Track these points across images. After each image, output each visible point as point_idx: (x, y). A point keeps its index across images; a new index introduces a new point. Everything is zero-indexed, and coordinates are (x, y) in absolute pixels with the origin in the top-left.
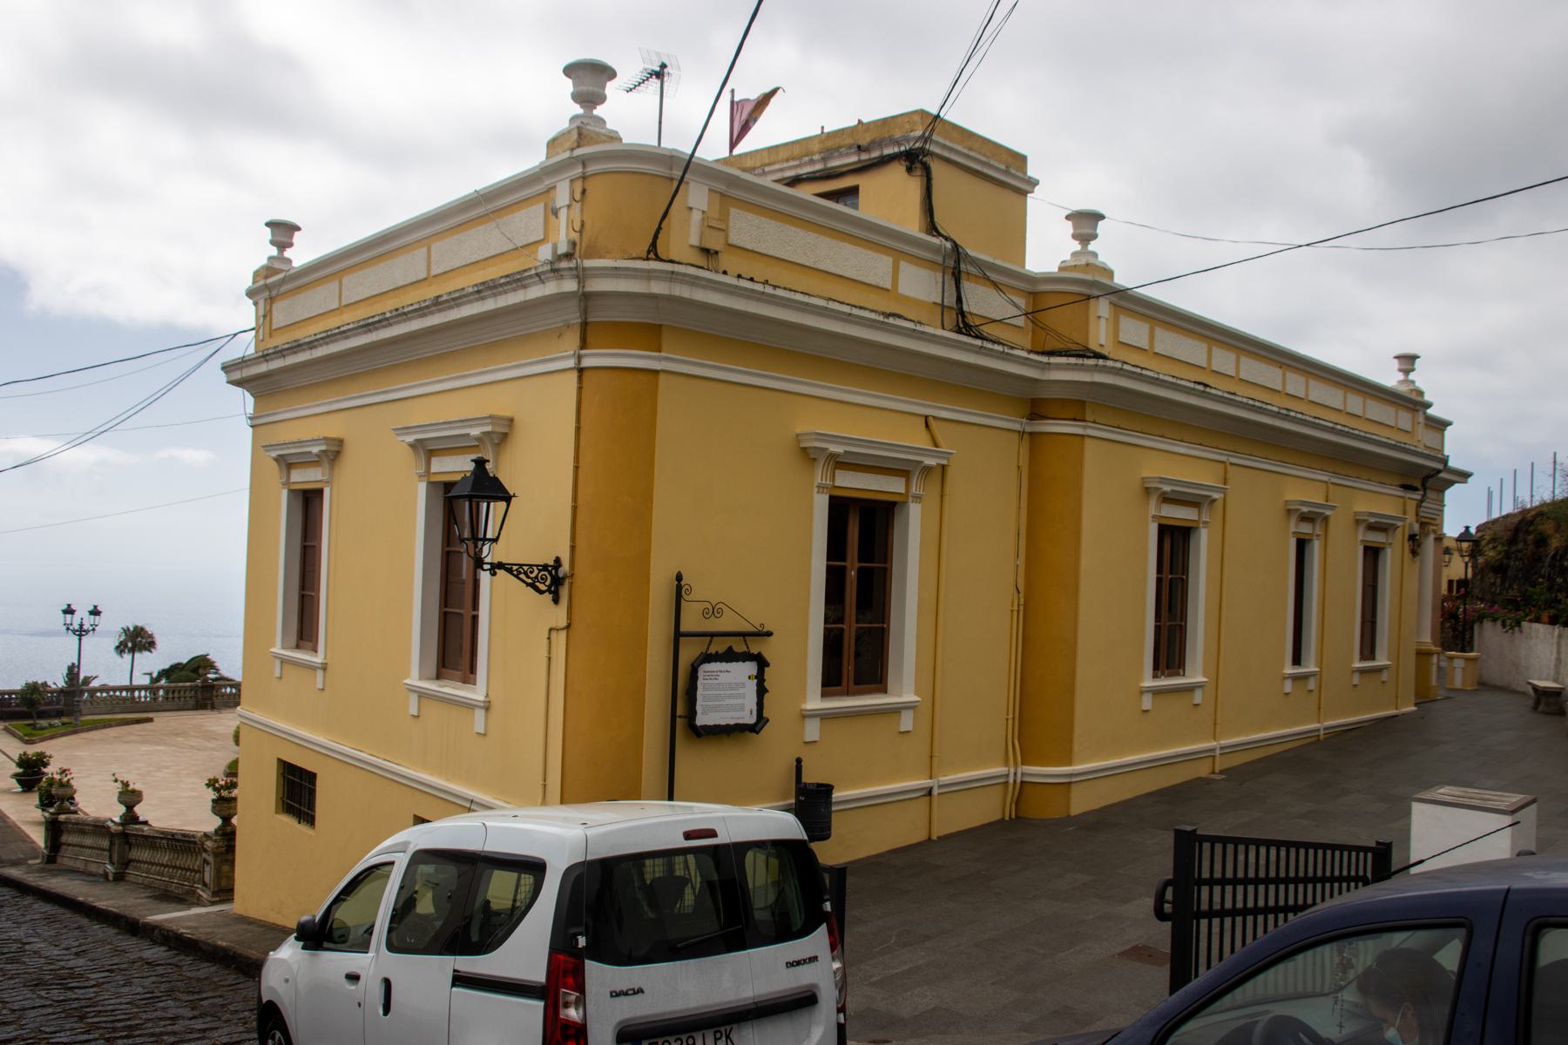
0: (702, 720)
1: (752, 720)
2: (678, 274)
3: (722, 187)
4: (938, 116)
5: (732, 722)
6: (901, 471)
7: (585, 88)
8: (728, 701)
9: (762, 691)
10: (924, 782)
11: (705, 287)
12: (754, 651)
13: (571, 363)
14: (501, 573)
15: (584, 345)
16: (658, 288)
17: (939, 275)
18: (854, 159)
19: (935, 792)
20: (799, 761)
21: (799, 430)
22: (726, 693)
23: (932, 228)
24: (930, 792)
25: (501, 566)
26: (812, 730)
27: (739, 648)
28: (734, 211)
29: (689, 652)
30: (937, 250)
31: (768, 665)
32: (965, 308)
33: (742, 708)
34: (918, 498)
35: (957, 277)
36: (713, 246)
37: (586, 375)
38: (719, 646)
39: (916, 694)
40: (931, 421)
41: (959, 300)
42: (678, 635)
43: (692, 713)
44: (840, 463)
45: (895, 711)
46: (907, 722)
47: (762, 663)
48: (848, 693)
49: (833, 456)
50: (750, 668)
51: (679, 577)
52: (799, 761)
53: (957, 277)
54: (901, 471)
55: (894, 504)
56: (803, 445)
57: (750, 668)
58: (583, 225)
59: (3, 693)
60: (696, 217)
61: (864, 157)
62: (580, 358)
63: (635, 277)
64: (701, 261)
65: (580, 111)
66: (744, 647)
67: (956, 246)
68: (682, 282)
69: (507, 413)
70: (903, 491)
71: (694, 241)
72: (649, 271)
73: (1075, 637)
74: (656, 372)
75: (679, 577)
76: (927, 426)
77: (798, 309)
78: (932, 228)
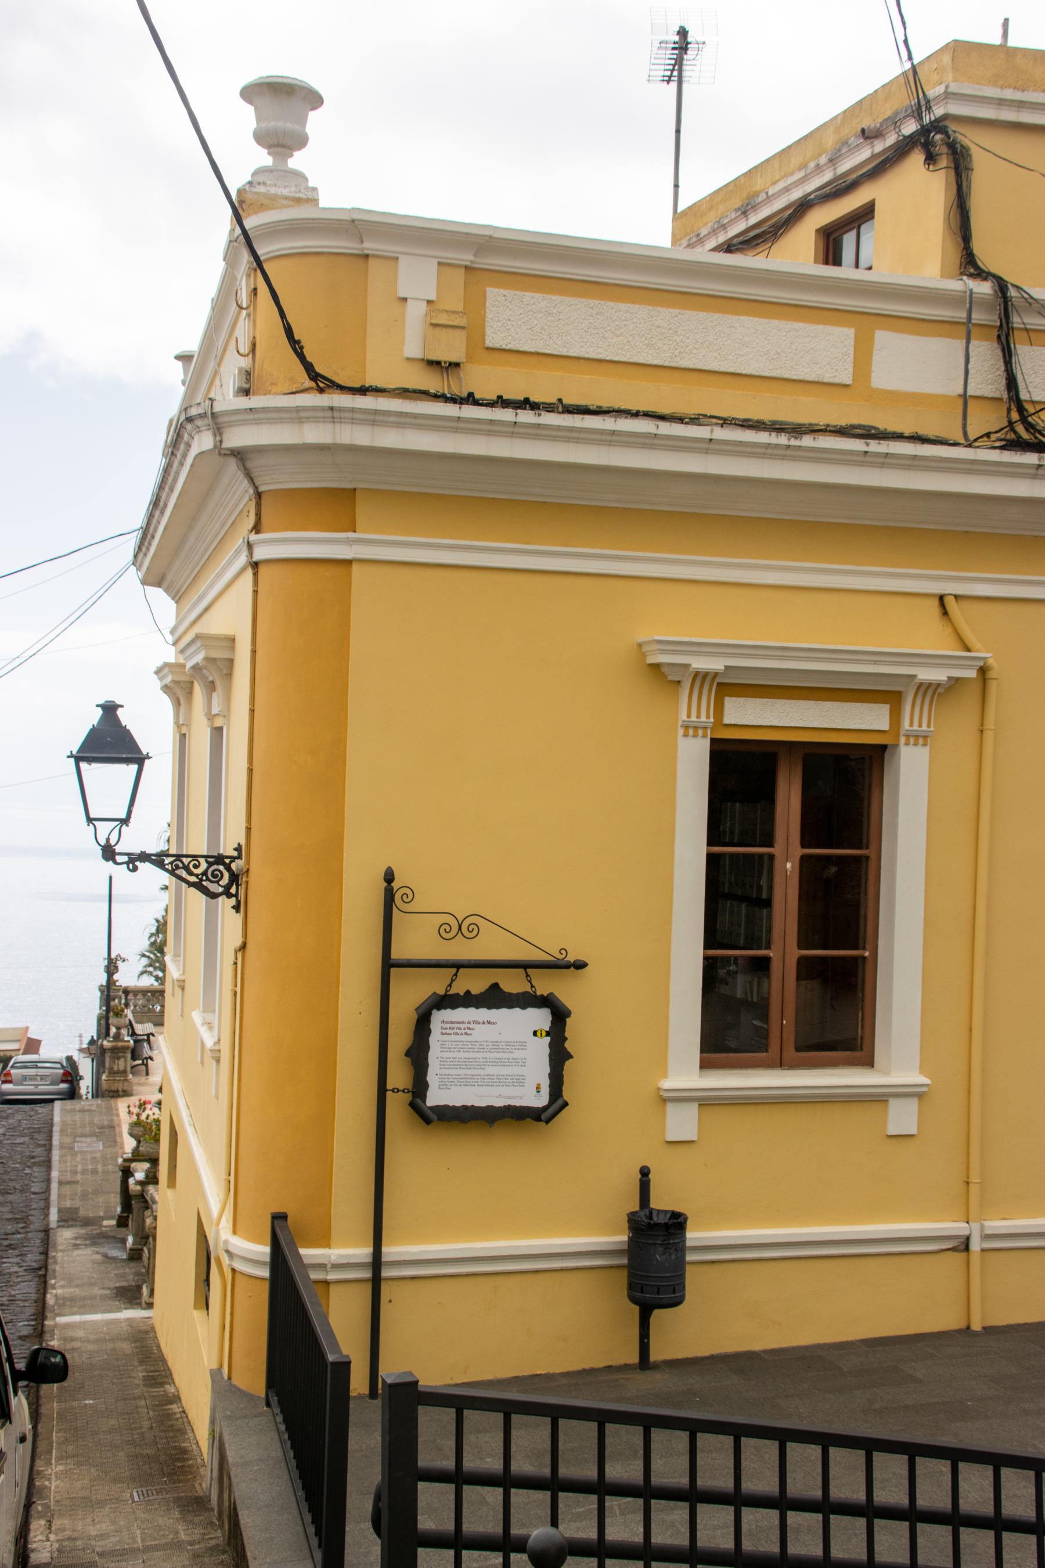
0: (435, 1098)
1: (541, 1101)
2: (340, 409)
3: (467, 257)
4: (914, 68)
5: (483, 1103)
6: (890, 696)
7: (273, 124)
8: (490, 1070)
9: (559, 1056)
10: (957, 1227)
11: (399, 425)
12: (542, 990)
13: (243, 559)
14: (144, 867)
15: (257, 528)
16: (314, 434)
17: (959, 345)
18: (865, 154)
19: (975, 1245)
20: (645, 1172)
21: (641, 638)
22: (488, 1056)
23: (969, 264)
24: (964, 1245)
25: (144, 857)
26: (682, 1123)
27: (512, 983)
28: (493, 294)
29: (409, 994)
30: (970, 301)
31: (568, 1014)
32: (1024, 396)
33: (520, 1081)
34: (920, 738)
35: (1005, 340)
36: (445, 356)
37: (262, 570)
38: (476, 983)
39: (922, 1071)
40: (950, 602)
41: (1011, 383)
42: (388, 964)
43: (419, 1087)
44: (726, 687)
45: (878, 1099)
46: (902, 1117)
47: (560, 1016)
48: (781, 1064)
49: (701, 678)
50: (540, 1018)
51: (389, 877)
52: (645, 1172)
53: (1005, 340)
54: (890, 696)
55: (884, 748)
56: (651, 660)
57: (540, 1018)
58: (254, 345)
59: (2, 1054)
60: (416, 312)
61: (879, 146)
62: (250, 546)
63: (281, 421)
64: (432, 382)
65: (267, 160)
66: (532, 985)
67: (1002, 286)
68: (353, 421)
69: (229, 632)
70: (885, 726)
71: (413, 348)
72: (298, 409)
73: (339, 961)
74: (348, 563)
75: (389, 877)
76: (945, 613)
77: (600, 443)
78: (969, 264)
